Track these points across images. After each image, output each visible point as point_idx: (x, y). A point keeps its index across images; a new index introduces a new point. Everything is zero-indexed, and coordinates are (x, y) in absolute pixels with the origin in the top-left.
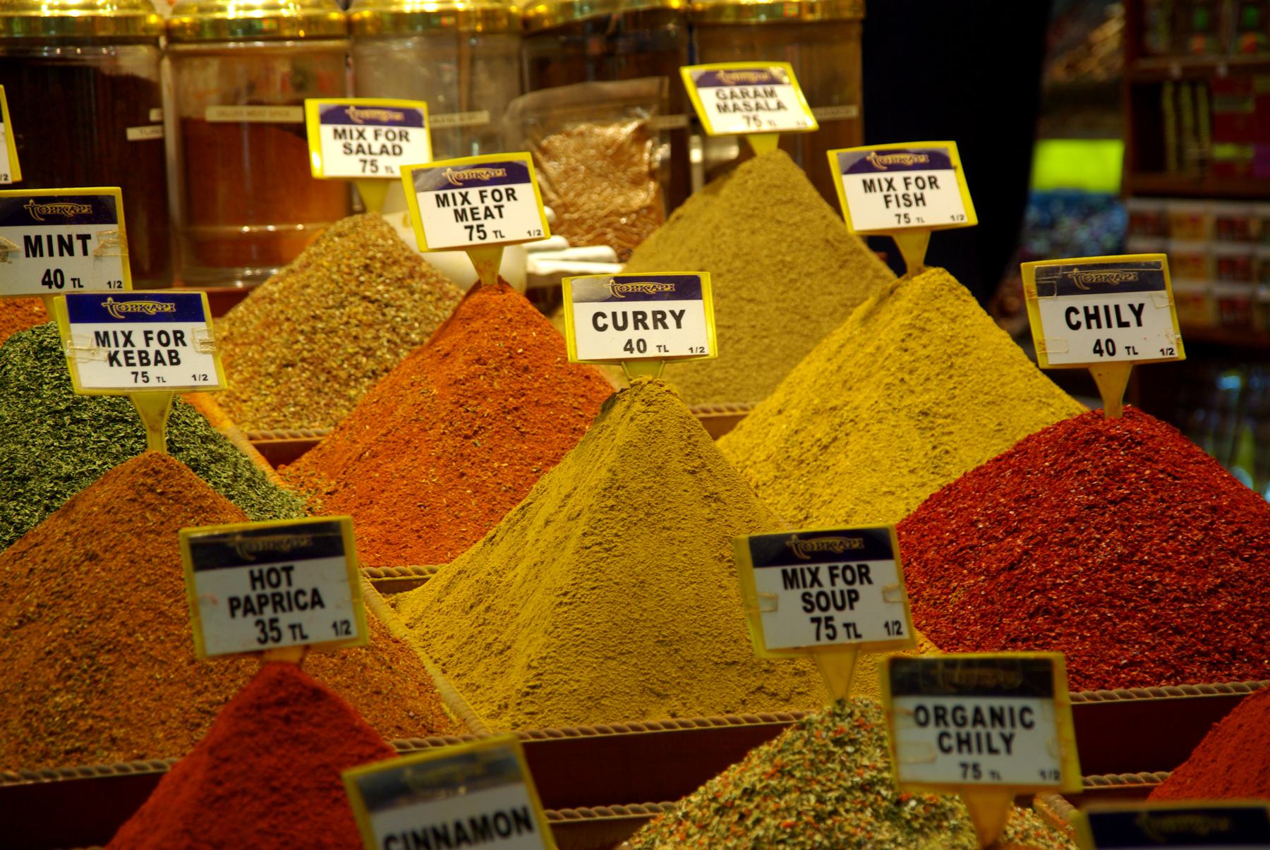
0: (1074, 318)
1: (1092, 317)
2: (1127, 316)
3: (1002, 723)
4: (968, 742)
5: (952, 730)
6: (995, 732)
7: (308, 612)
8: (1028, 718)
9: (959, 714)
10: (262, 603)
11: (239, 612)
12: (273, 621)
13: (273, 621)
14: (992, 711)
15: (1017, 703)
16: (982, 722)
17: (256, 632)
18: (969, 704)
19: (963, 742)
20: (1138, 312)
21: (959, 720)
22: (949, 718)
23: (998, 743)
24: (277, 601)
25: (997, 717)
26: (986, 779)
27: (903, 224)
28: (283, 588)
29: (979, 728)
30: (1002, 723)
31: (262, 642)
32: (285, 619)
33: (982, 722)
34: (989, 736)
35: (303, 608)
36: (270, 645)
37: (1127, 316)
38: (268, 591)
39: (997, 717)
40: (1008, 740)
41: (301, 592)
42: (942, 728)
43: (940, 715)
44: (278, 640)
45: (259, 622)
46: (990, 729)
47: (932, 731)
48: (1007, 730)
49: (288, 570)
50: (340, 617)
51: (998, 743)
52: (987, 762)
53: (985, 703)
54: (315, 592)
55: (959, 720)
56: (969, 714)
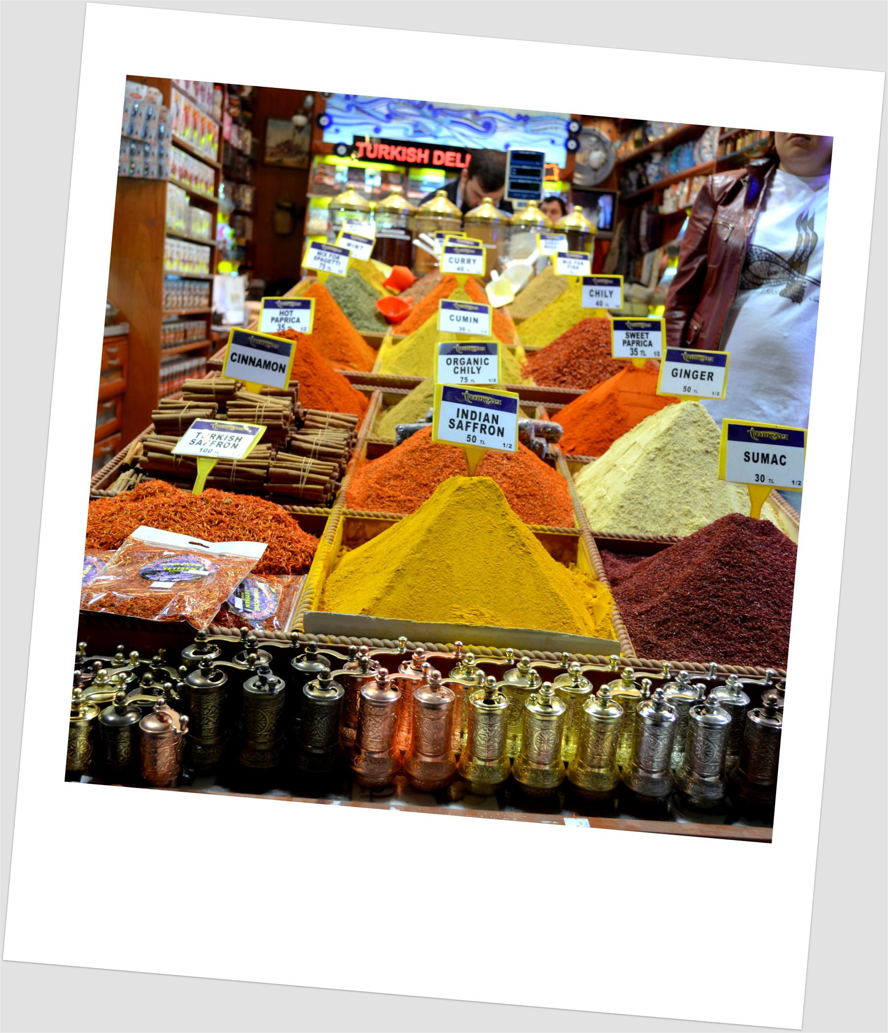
0: (592, 293)
1: (597, 293)
2: (608, 294)
3: (477, 363)
4: (464, 370)
5: (459, 366)
6: (475, 367)
7: (647, 347)
8: (487, 362)
9: (695, 373)
10: (282, 319)
11: (626, 345)
12: (636, 349)
13: (636, 349)
14: (475, 360)
15: (484, 357)
16: (470, 363)
17: (630, 352)
18: (466, 357)
19: (463, 370)
20: (611, 293)
21: (695, 376)
22: (459, 362)
23: (475, 370)
24: (286, 320)
25: (476, 361)
26: (469, 382)
27: (460, 272)
28: (289, 316)
29: (469, 365)
30: (477, 363)
31: (632, 355)
32: (640, 349)
33: (470, 363)
34: (472, 368)
35: (646, 346)
36: (634, 356)
37: (608, 294)
38: (636, 339)
39: (476, 361)
40: (479, 369)
41: (294, 318)
42: (456, 365)
43: (456, 361)
44: (636, 355)
45: (632, 349)
46: (473, 365)
47: (452, 366)
48: (479, 366)
49: (291, 312)
50: (657, 350)
51: (475, 370)
52: (470, 376)
53: (472, 357)
54: (650, 342)
55: (695, 376)
56: (466, 361)
